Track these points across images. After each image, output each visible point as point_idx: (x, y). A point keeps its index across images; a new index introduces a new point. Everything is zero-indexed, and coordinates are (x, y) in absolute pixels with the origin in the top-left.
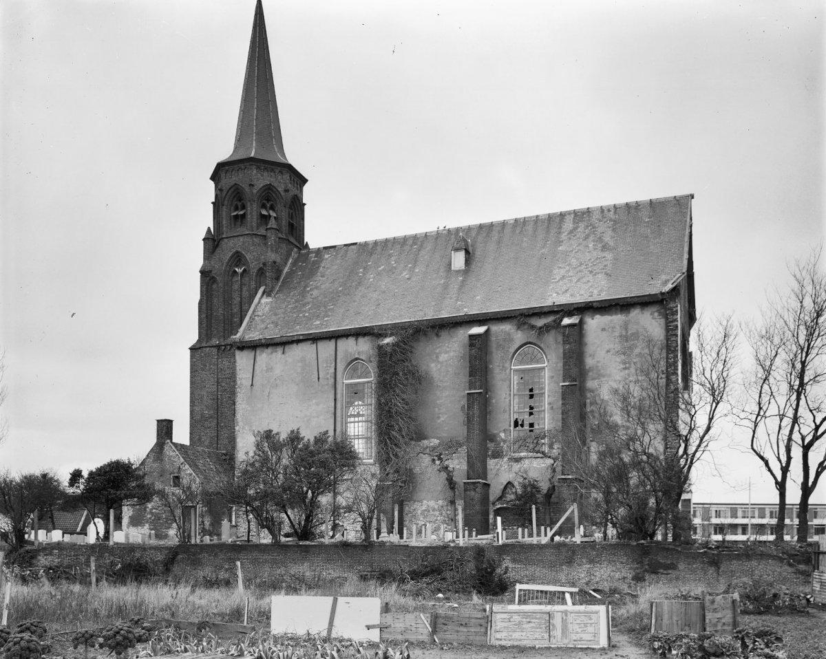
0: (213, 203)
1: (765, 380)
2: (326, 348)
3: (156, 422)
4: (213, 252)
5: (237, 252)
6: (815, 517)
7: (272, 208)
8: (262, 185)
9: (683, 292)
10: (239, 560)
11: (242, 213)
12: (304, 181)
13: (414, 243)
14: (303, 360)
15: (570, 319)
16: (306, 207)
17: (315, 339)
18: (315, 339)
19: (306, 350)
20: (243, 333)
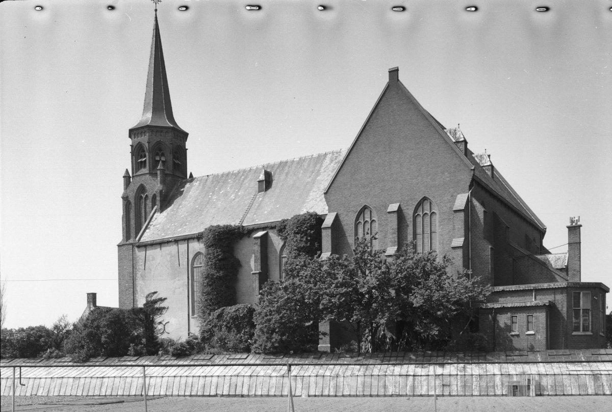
0: (568, 227)
1: (530, 257)
2: (183, 247)
3: (86, 295)
4: (126, 188)
5: (142, 185)
6: (528, 330)
7: (163, 155)
8: (155, 142)
9: (500, 210)
10: (436, 313)
11: (144, 159)
12: (185, 135)
13: (243, 175)
14: (170, 254)
15: (408, 226)
16: (187, 151)
17: (177, 241)
18: (177, 241)
19: (173, 248)
20: (148, 236)
